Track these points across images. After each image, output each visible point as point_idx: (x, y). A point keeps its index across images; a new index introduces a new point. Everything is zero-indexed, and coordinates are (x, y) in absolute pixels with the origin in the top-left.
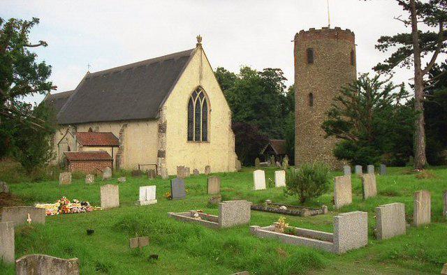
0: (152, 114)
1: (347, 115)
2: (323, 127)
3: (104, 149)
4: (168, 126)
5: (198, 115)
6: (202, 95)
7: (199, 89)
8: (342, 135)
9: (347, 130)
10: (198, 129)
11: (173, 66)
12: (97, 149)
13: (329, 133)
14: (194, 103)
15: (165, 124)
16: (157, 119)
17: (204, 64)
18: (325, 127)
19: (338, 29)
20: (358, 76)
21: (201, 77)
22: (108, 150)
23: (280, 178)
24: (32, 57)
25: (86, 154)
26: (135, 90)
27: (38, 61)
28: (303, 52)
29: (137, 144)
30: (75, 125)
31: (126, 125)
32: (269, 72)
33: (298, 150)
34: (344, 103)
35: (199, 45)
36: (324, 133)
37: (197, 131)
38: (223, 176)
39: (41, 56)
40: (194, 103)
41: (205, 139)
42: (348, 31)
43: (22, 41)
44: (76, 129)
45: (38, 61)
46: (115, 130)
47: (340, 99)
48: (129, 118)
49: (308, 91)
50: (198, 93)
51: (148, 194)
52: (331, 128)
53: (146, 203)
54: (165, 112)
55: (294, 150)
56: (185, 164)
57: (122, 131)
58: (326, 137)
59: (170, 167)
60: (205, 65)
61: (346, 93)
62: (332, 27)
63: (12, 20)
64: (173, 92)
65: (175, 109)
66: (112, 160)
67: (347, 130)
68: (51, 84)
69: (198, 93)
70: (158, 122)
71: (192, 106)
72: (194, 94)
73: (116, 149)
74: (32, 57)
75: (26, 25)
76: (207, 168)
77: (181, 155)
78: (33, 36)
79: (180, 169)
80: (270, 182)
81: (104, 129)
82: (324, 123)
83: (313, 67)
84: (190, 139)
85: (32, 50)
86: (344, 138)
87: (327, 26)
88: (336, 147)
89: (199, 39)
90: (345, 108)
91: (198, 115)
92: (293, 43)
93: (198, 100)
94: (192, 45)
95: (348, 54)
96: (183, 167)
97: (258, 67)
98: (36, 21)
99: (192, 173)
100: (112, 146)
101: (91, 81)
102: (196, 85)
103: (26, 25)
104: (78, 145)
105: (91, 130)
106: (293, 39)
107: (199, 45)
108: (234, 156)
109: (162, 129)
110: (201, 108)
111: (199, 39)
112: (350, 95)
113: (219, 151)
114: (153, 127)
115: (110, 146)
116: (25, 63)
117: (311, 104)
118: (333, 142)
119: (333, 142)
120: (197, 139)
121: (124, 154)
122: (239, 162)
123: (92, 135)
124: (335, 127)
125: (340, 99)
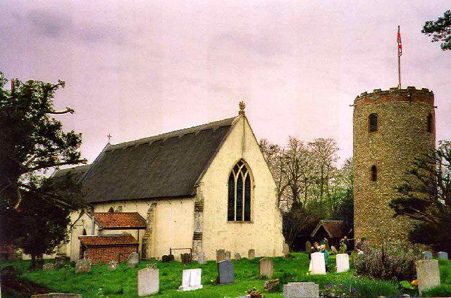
0: (188, 192)
1: (423, 191)
2: (391, 205)
3: (127, 231)
4: (206, 204)
5: (240, 192)
6: (244, 170)
7: (241, 162)
8: (416, 215)
9: (423, 210)
10: (239, 207)
11: (214, 136)
12: (120, 232)
13: (399, 213)
14: (244, 179)
15: (202, 202)
16: (194, 196)
17: (246, 131)
18: (395, 204)
19: (412, 89)
20: (437, 146)
21: (243, 149)
22: (133, 233)
23: (343, 262)
24: (58, 126)
25: (107, 238)
26: (171, 164)
27: (66, 130)
28: (365, 121)
29: (171, 226)
30: (94, 204)
31: (155, 204)
32: (320, 144)
33: (359, 233)
34: (419, 178)
35: (242, 113)
36: (393, 212)
37: (239, 209)
38: (276, 261)
39: (68, 126)
40: (244, 179)
41: (248, 219)
42: (425, 91)
43: (44, 108)
44: (93, 209)
45: (66, 130)
46: (142, 209)
47: (414, 172)
48: (159, 195)
49: (370, 164)
50: (241, 166)
51: (192, 279)
52: (401, 207)
53: (189, 289)
54: (202, 188)
55: (353, 231)
56: (227, 247)
57: (151, 210)
58: (395, 216)
59: (208, 252)
60: (249, 136)
61: (423, 165)
62: (404, 87)
63: (31, 82)
64: (212, 165)
65: (214, 185)
66: (138, 245)
67: (423, 210)
68: (78, 157)
69: (241, 166)
70: (195, 200)
71: (242, 180)
72: (236, 168)
73: (142, 232)
74: (58, 126)
75: (48, 89)
76: (251, 251)
77: (225, 238)
78: (58, 101)
79: (220, 253)
80: (330, 266)
81: (129, 208)
82: (392, 201)
83: (377, 136)
84: (230, 218)
85: (58, 118)
86: (420, 219)
87: (396, 86)
88: (413, 229)
89: (242, 106)
90: (420, 183)
91: (240, 192)
92: (435, 105)
93: (240, 174)
94: (233, 112)
95: (423, 119)
96: (224, 251)
97: (307, 138)
98: (62, 84)
99: (233, 257)
100: (138, 228)
101: (113, 155)
102: (238, 158)
103: (48, 89)
104: (97, 227)
105: (111, 210)
106: (352, 104)
107: (242, 113)
108: (281, 239)
109: (199, 208)
110: (236, 184)
111: (242, 106)
112: (427, 169)
113: (265, 235)
114: (189, 205)
115: (134, 228)
116: (50, 131)
117: (374, 178)
118: (407, 223)
119: (407, 223)
120: (239, 219)
121: (153, 237)
122: (287, 246)
123: (114, 216)
124: (404, 207)
125: (414, 172)
